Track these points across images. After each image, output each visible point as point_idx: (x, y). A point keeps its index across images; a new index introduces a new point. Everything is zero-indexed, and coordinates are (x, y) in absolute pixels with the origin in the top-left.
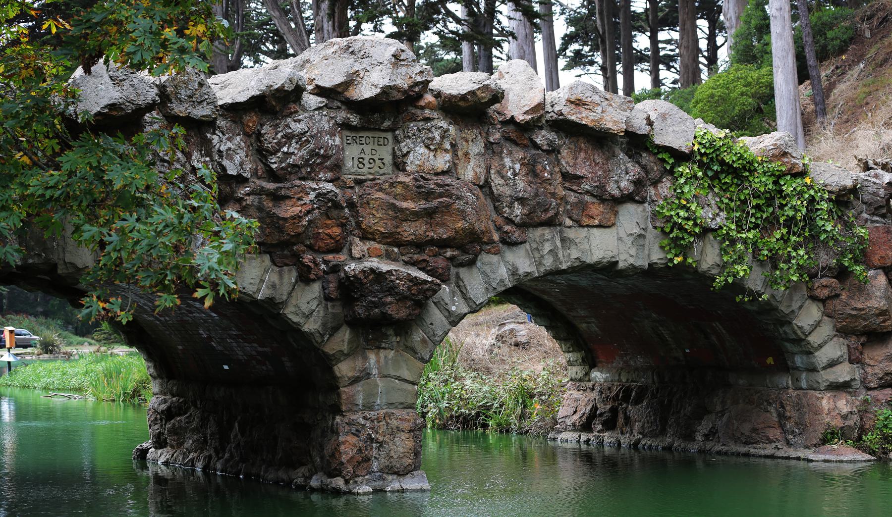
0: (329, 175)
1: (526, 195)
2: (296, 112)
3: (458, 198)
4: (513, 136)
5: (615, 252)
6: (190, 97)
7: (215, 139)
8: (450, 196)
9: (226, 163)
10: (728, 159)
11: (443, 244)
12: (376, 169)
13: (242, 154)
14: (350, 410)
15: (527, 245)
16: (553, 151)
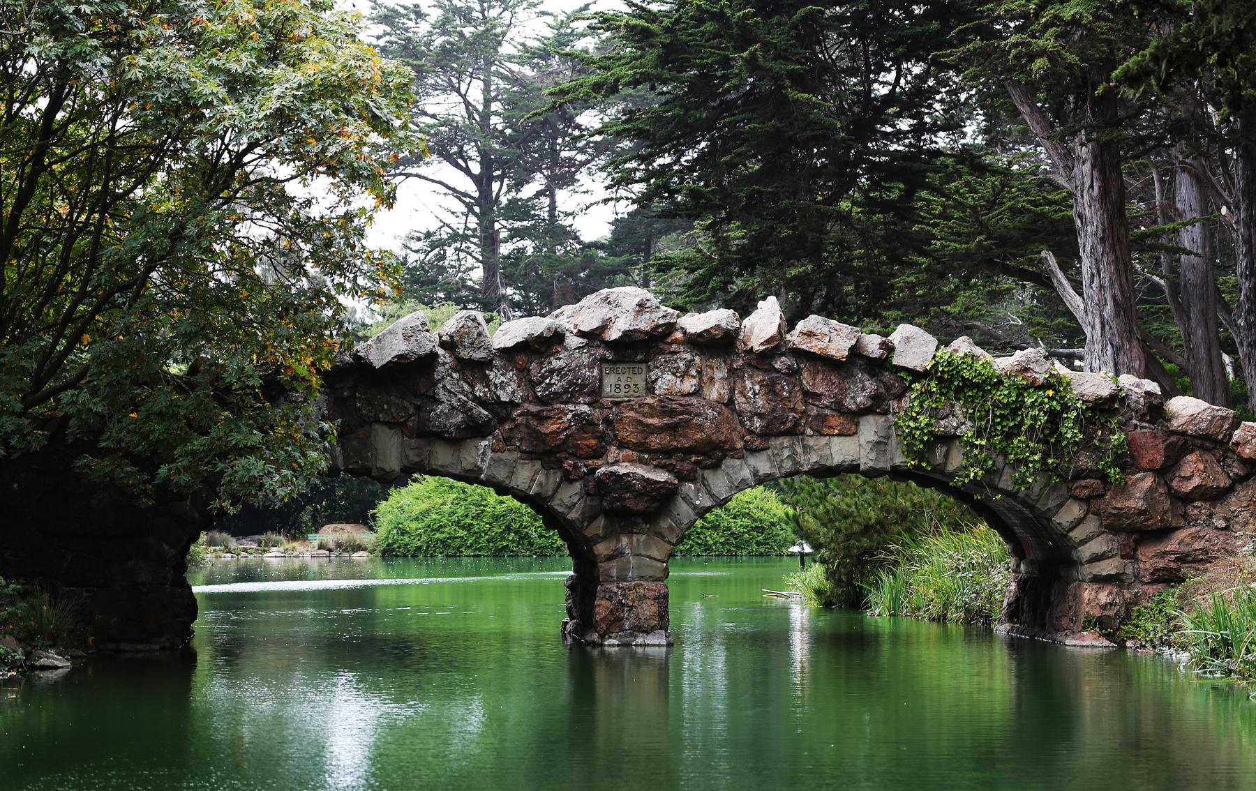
0: (587, 399)
1: (763, 411)
2: (558, 352)
3: (697, 415)
4: (753, 363)
5: (855, 457)
6: (471, 344)
7: (492, 375)
8: (689, 414)
9: (500, 392)
10: (966, 374)
11: (688, 451)
12: (631, 392)
13: (514, 385)
14: (607, 581)
15: (769, 452)
16: (793, 373)
